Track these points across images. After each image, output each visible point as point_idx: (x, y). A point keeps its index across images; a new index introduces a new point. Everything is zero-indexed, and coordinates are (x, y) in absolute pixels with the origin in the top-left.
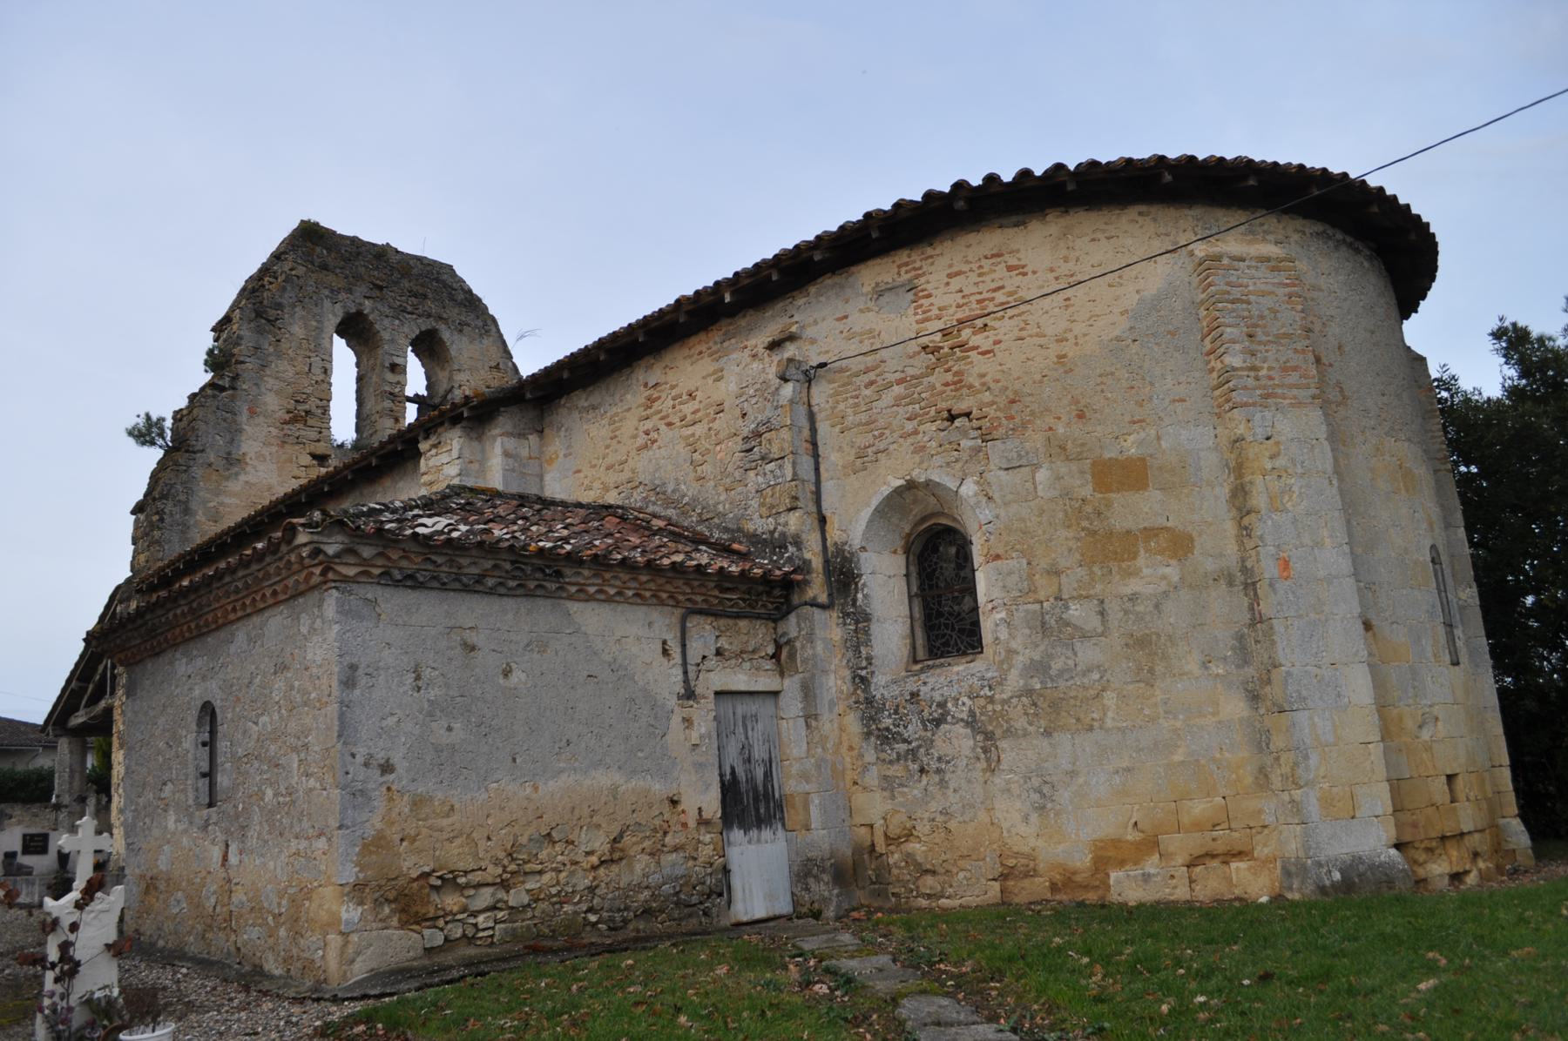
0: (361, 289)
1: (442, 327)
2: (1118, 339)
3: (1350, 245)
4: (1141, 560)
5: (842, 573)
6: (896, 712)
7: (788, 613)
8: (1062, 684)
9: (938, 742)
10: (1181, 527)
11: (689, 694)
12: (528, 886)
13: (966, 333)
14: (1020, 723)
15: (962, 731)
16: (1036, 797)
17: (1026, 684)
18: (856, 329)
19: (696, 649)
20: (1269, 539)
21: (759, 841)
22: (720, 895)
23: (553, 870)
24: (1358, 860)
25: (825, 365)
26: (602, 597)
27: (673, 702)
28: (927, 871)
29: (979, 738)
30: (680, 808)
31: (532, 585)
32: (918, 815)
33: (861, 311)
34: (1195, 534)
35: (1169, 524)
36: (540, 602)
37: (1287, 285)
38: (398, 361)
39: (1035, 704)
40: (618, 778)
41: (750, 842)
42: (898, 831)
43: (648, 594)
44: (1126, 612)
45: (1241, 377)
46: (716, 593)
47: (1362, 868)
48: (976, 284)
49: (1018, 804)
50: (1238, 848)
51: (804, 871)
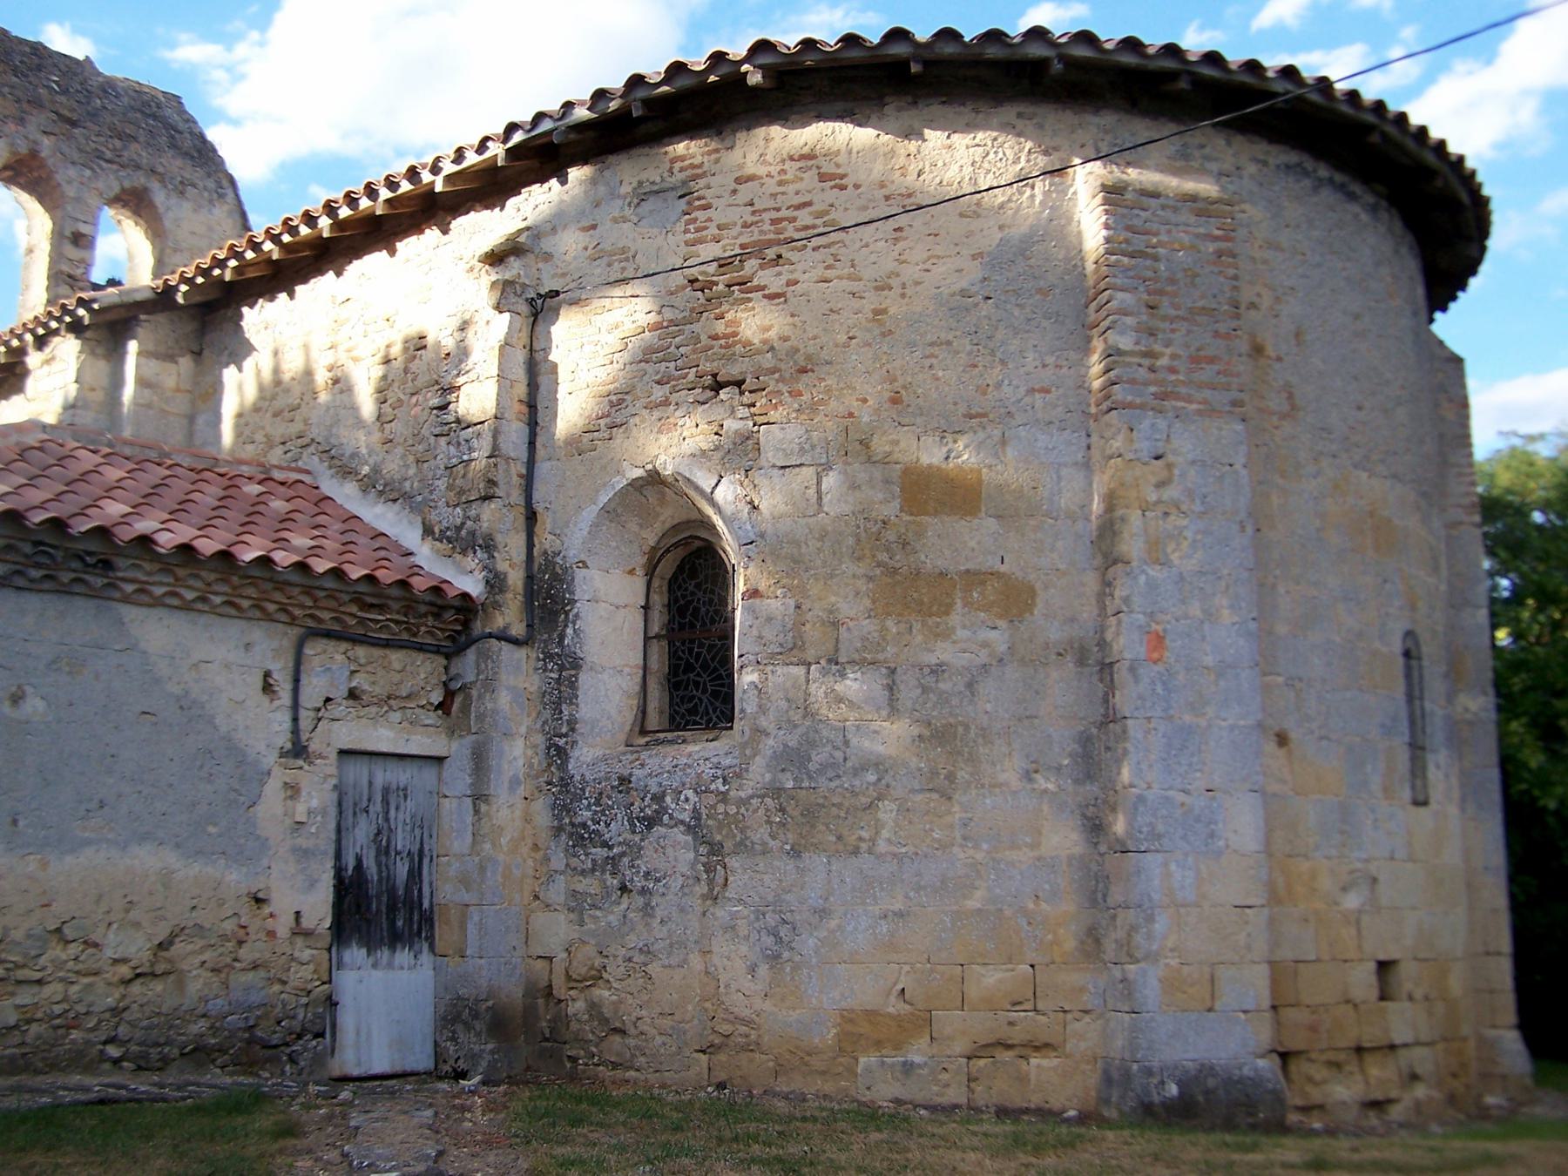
0: (37, 120)
1: (155, 185)
2: (964, 294)
3: (1341, 187)
4: (955, 619)
5: (549, 596)
6: (598, 803)
7: (468, 646)
8: (823, 783)
9: (648, 852)
10: (1019, 574)
11: (298, 750)
12: (19, 1001)
13: (751, 264)
14: (760, 834)
15: (682, 838)
16: (769, 941)
17: (773, 780)
18: (606, 246)
19: (314, 688)
20: (1137, 601)
21: (390, 966)
22: (321, 1035)
23: (62, 980)
24: (1206, 1070)
25: (557, 293)
26: (175, 602)
27: (271, 759)
28: (616, 1030)
29: (703, 850)
30: (267, 910)
31: (66, 577)
32: (611, 950)
33: (615, 220)
34: (1038, 586)
35: (1003, 569)
36: (80, 602)
37: (1216, 239)
38: (84, 229)
39: (782, 810)
40: (171, 858)
41: (375, 966)
42: (583, 970)
43: (245, 603)
44: (925, 690)
45: (1129, 365)
46: (354, 609)
47: (1211, 1083)
48: (774, 196)
49: (744, 949)
50: (1044, 1038)
51: (455, 1015)
